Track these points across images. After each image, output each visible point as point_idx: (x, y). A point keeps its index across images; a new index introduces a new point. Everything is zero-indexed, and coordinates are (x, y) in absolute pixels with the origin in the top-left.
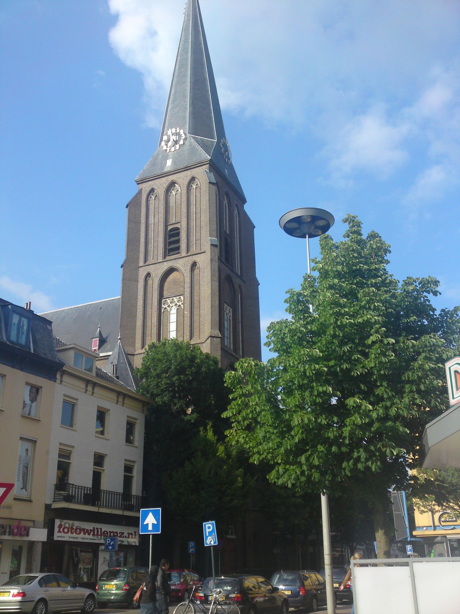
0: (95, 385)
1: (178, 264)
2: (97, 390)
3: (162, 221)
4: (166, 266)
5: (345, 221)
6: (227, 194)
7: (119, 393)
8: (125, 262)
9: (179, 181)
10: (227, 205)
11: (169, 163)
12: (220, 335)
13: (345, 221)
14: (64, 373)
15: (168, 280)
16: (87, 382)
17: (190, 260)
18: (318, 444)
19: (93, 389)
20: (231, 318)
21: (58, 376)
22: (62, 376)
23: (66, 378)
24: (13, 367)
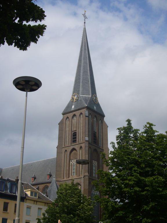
0: (37, 201)
1: (76, 147)
2: (38, 203)
3: (71, 129)
4: (72, 147)
5: (111, 143)
6: (95, 116)
7: (45, 203)
8: (58, 146)
9: (76, 114)
10: (96, 120)
11: (73, 107)
12: (88, 175)
13: (111, 143)
14: (26, 199)
15: (73, 152)
16: (34, 201)
17: (80, 145)
18: (60, 219)
19: (37, 203)
20: (97, 165)
21: (25, 201)
22: (26, 200)
23: (27, 201)
24: (11, 200)
